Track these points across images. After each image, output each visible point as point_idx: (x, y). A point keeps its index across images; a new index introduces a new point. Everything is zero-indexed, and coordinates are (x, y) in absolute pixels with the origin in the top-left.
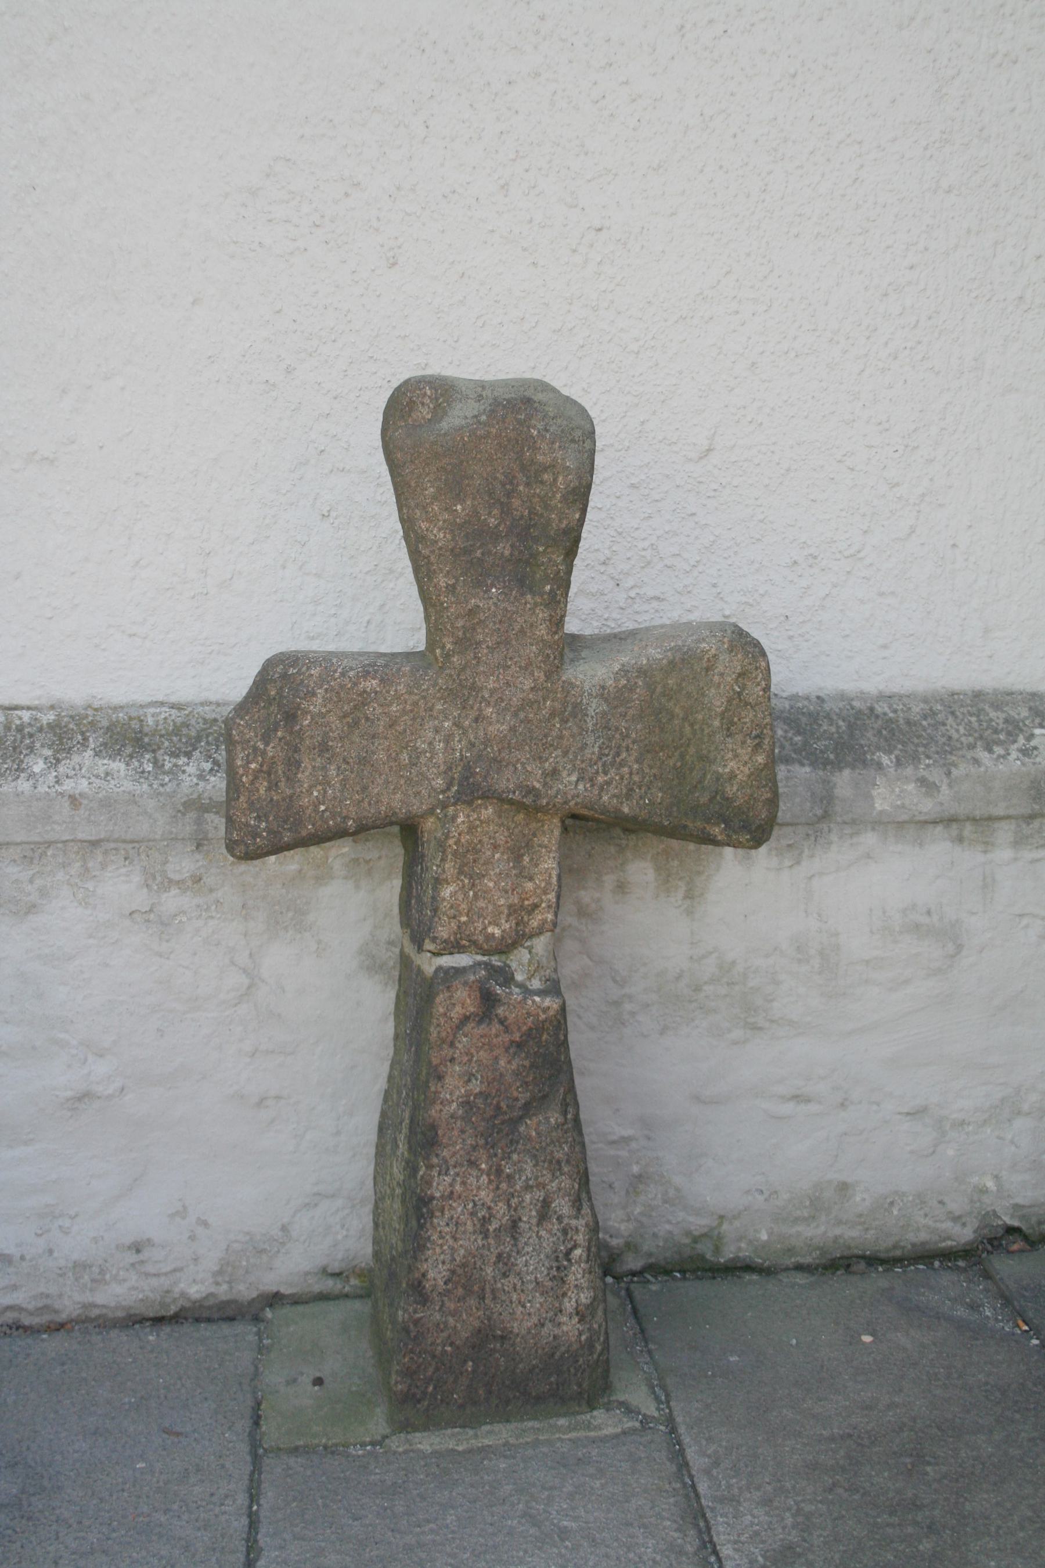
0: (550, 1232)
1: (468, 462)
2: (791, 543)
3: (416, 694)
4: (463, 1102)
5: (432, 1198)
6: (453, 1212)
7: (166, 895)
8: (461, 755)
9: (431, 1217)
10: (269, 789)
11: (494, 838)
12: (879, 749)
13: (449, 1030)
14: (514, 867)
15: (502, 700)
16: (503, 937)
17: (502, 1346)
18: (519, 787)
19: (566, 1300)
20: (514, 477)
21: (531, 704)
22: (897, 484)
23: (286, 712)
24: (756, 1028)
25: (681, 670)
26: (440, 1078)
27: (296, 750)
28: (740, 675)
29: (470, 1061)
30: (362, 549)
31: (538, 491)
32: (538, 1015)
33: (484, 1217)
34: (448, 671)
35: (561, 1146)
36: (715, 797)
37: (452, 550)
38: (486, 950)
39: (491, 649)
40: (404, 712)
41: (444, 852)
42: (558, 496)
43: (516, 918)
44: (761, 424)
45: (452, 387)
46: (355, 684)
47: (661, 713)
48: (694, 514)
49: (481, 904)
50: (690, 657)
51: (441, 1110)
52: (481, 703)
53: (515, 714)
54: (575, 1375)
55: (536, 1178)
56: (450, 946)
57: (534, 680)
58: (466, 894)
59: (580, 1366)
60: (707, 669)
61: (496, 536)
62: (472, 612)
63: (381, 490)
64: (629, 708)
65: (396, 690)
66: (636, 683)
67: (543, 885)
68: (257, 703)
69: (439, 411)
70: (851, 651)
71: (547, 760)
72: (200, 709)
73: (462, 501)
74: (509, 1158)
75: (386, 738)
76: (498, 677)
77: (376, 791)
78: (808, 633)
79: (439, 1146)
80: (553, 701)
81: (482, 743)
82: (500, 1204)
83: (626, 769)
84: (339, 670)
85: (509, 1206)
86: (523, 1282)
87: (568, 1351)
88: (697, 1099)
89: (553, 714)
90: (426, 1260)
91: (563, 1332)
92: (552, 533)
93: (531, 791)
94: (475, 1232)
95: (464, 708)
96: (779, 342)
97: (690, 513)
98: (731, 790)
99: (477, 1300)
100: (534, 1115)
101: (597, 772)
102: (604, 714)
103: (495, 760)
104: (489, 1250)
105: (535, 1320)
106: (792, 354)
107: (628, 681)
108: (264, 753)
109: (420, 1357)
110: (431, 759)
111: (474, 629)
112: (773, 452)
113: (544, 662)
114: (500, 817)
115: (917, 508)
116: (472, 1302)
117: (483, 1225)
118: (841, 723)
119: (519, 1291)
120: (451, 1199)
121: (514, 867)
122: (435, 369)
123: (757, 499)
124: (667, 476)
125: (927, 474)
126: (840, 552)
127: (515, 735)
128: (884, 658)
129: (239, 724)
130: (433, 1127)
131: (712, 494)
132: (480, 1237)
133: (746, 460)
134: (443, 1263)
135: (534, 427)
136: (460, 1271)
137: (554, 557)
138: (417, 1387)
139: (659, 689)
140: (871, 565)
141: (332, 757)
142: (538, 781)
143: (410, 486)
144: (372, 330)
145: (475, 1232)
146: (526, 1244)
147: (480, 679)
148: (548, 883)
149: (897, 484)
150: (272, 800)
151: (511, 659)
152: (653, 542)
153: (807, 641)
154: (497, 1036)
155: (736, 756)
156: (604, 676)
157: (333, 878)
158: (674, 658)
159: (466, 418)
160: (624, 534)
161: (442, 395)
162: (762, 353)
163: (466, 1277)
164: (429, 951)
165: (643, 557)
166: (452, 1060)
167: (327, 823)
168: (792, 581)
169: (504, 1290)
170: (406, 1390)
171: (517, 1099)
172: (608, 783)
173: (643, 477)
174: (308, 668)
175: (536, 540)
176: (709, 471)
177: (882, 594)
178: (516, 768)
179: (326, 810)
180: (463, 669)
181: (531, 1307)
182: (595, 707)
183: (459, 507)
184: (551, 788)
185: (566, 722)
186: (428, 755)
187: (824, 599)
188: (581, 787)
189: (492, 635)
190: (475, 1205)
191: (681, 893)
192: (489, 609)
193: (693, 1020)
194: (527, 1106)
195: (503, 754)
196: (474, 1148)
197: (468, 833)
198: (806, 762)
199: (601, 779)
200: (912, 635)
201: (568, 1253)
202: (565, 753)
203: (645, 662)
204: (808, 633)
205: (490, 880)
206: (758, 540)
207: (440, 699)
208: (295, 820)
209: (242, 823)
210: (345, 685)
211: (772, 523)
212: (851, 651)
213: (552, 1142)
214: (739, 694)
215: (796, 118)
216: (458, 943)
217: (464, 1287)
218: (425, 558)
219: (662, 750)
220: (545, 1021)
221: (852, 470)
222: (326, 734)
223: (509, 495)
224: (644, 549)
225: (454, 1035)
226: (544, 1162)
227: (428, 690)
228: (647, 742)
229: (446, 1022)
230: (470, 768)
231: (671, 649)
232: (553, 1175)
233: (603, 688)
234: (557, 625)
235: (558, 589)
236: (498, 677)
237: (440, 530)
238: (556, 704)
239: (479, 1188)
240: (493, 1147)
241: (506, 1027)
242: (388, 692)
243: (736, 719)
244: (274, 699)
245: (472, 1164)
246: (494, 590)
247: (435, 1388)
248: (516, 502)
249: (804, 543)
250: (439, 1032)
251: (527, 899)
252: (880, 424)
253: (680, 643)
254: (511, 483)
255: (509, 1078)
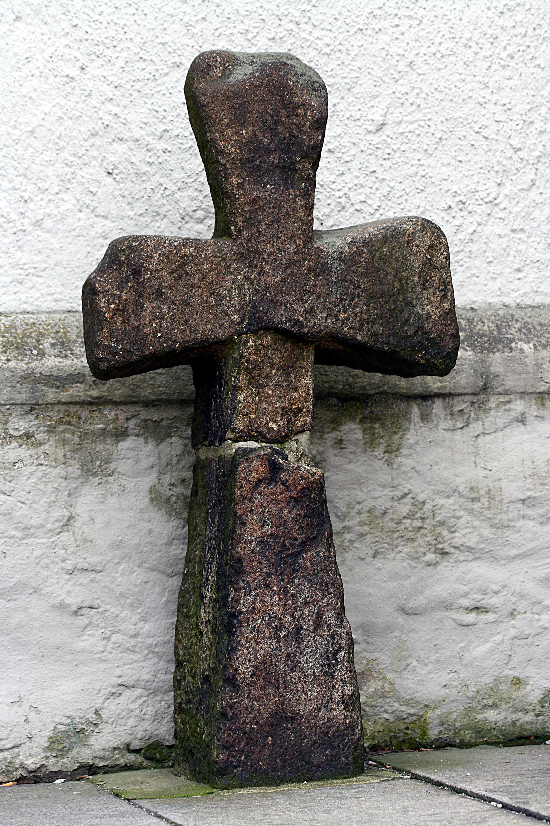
0: (322, 637)
1: (248, 102)
2: (446, 192)
3: (219, 257)
4: (259, 542)
5: (241, 612)
6: (255, 623)
7: (8, 447)
8: (250, 298)
9: (240, 627)
10: (123, 322)
11: (272, 359)
12: (521, 340)
13: (248, 490)
14: (285, 380)
15: (276, 260)
16: (279, 431)
17: (292, 725)
18: (289, 320)
19: (335, 691)
20: (279, 112)
21: (294, 263)
22: (520, 149)
23: (134, 269)
24: (444, 553)
25: (391, 242)
26: (244, 524)
27: (141, 296)
28: (430, 247)
29: (264, 511)
30: (137, 197)
31: (295, 121)
32: (309, 478)
33: (276, 626)
34: (239, 241)
35: (327, 573)
36: (417, 331)
37: (241, 160)
38: (268, 439)
39: (268, 226)
40: (212, 270)
41: (239, 367)
42: (308, 124)
43: (287, 418)
44: (419, 106)
45: (234, 56)
46: (179, 250)
47: (379, 271)
48: (374, 172)
49: (264, 405)
50: (397, 233)
51: (245, 548)
52: (262, 262)
53: (285, 270)
54: (343, 750)
55: (312, 596)
56: (244, 435)
57: (297, 246)
58: (254, 400)
59: (346, 743)
60: (408, 242)
61: (269, 151)
62: (254, 201)
63: (150, 154)
64: (359, 267)
65: (206, 254)
66: (362, 250)
67: (304, 395)
68: (111, 267)
69: (226, 73)
70: (494, 273)
71: (307, 301)
72: (21, 316)
73: (246, 129)
74: (293, 582)
75: (200, 287)
76: (273, 244)
77: (194, 323)
78: (462, 260)
79: (245, 573)
80: (309, 261)
81: (264, 290)
82: (288, 617)
83: (358, 310)
84: (167, 242)
85: (294, 617)
86: (305, 675)
87: (337, 731)
88: (404, 611)
89: (310, 270)
90: (238, 658)
91: (333, 715)
92: (305, 148)
93: (297, 322)
94: (270, 638)
95: (251, 266)
96: (429, 47)
97: (371, 170)
98: (429, 326)
99: (274, 689)
100: (308, 550)
101: (339, 311)
102: (343, 271)
103: (272, 301)
104: (281, 651)
105: (314, 705)
106: (439, 55)
107: (357, 248)
108: (120, 297)
109: (236, 733)
110: (230, 301)
111: (256, 212)
112: (429, 126)
113: (303, 235)
114: (275, 343)
115: (535, 166)
116: (270, 690)
117: (276, 633)
118: (490, 325)
119: (303, 683)
120: (253, 613)
121: (285, 380)
122: (221, 45)
123: (419, 160)
124: (354, 144)
125: (541, 141)
126: (482, 199)
127: (285, 284)
128: (519, 279)
129: (100, 280)
130: (240, 560)
131: (387, 156)
132: (274, 641)
133: (410, 132)
134: (250, 661)
135: (290, 80)
136: (261, 667)
137: (306, 164)
138: (234, 757)
139: (377, 255)
140: (505, 209)
141: (165, 299)
142: (302, 316)
143: (212, 118)
144: (142, 38)
145: (270, 638)
146: (306, 646)
147: (261, 246)
148: (308, 394)
149: (520, 149)
150: (125, 329)
151: (281, 232)
152: (346, 192)
153: (461, 266)
154: (281, 494)
155: (430, 302)
156: (342, 245)
157: (128, 436)
158: (386, 234)
159: (246, 75)
160: (325, 187)
161: (228, 62)
162: (418, 54)
163: (265, 671)
164: (230, 439)
165: (340, 203)
166: (251, 511)
167: (162, 346)
168: (448, 221)
169: (292, 682)
170: (225, 758)
171: (296, 539)
172: (347, 319)
173: (337, 144)
174: (146, 241)
175: (295, 153)
176: (384, 140)
177: (514, 231)
178: (287, 307)
179: (161, 336)
180: (249, 240)
181: (311, 694)
182: (336, 267)
183: (244, 132)
184: (310, 321)
185: (318, 276)
186: (228, 298)
187: (472, 234)
188: (329, 321)
189: (268, 216)
190: (270, 617)
191: (382, 449)
192: (266, 198)
193: (397, 546)
194: (303, 543)
195: (278, 298)
196: (268, 574)
197: (255, 354)
198: (468, 348)
199: (342, 316)
200: (538, 261)
201: (335, 654)
202: (319, 297)
203: (367, 237)
204: (462, 260)
205: (270, 389)
206: (422, 190)
207: (235, 260)
208: (141, 343)
209: (106, 346)
210: (172, 251)
211: (431, 177)
212: (494, 273)
213: (322, 570)
214: (430, 260)
215: (131, 39)
216: (249, 433)
217: (264, 679)
218: (223, 165)
219: (381, 297)
220: (312, 483)
221: (486, 138)
222: (160, 284)
223: (276, 123)
224: (340, 197)
225: (252, 493)
226: (317, 584)
227: (227, 254)
228: (371, 291)
229: (246, 484)
230: (256, 307)
231: (383, 228)
232: (323, 594)
233: (341, 253)
234: (310, 210)
235: (310, 186)
236: (273, 244)
237: (232, 146)
238: (311, 263)
239: (272, 605)
240: (280, 574)
241: (287, 487)
242: (200, 255)
243: (428, 278)
244: (124, 262)
245: (267, 586)
246: (268, 186)
247: (246, 758)
248: (280, 129)
249: (456, 192)
250: (241, 492)
251: (294, 404)
252: (504, 105)
253: (389, 224)
254: (277, 116)
255: (290, 524)
